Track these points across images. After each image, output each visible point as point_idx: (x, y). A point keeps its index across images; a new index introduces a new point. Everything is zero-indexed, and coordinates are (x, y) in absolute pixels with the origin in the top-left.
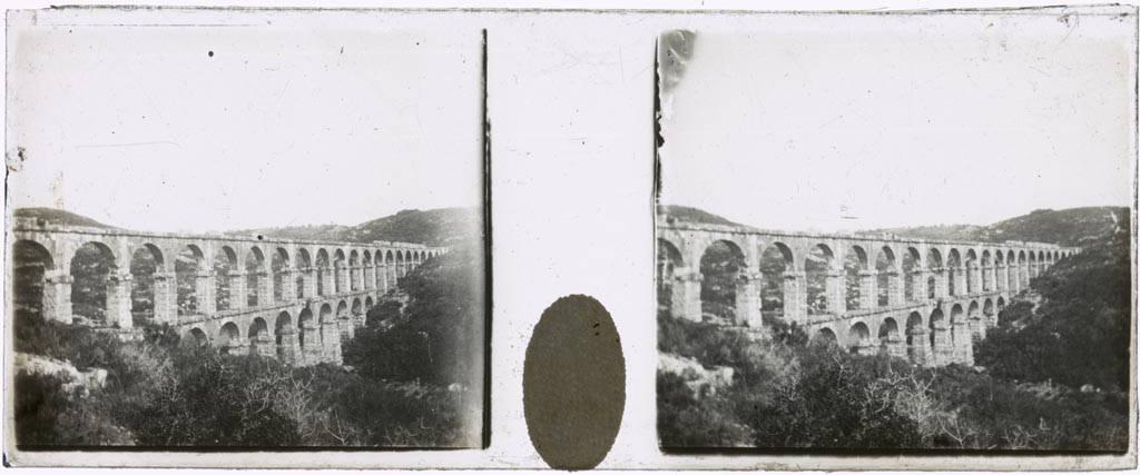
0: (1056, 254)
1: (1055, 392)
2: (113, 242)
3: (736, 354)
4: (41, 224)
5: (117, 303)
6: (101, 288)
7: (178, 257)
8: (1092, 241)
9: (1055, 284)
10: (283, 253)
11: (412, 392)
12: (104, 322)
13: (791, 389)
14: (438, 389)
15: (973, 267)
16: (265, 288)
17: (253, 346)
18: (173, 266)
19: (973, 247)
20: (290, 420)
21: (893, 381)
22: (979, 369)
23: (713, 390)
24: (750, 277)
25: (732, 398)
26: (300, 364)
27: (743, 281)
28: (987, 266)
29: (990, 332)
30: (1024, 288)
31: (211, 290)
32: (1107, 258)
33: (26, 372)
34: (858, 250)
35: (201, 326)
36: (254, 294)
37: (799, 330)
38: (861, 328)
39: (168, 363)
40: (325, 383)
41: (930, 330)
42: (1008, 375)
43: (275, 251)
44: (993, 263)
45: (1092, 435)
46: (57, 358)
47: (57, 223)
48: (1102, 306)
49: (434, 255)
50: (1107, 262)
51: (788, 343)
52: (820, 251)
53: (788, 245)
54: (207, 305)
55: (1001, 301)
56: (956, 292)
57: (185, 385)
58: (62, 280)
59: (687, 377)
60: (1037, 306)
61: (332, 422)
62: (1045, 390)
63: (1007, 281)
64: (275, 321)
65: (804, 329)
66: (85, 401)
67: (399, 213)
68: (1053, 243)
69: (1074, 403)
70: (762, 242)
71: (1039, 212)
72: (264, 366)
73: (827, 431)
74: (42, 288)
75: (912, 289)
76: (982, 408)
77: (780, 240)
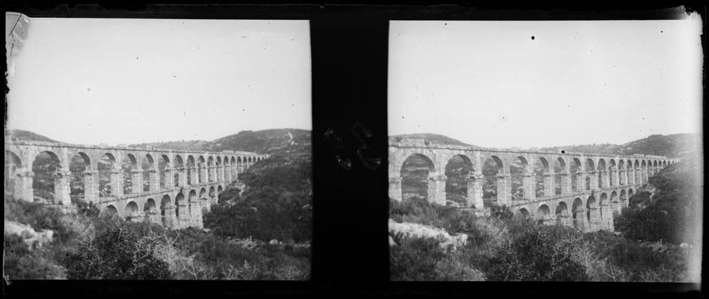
0: (254, 158)
1: (254, 244)
3: (55, 222)
4: (427, 144)
5: (61, 189)
6: (51, 180)
7: (512, 164)
8: (277, 150)
9: (253, 178)
10: (577, 162)
11: (657, 248)
12: (465, 205)
13: (89, 244)
14: (673, 247)
15: (203, 167)
16: (566, 183)
17: (558, 220)
18: (509, 170)
20: (581, 266)
21: (152, 238)
22: (207, 230)
23: (40, 244)
24: (63, 174)
25: (52, 249)
26: (588, 231)
27: (59, 176)
28: (211, 166)
29: (213, 207)
30: (234, 180)
31: (121, 182)
32: (285, 161)
33: (417, 235)
34: (131, 156)
35: (526, 207)
36: (147, 184)
37: (94, 207)
38: (133, 205)
39: (505, 230)
40: (603, 242)
41: (176, 207)
42: (225, 234)
43: (573, 161)
44: (215, 164)
45: (277, 271)
46: (436, 227)
47: (24, 139)
48: (283, 191)
49: (671, 162)
50: (286, 163)
51: (87, 215)
52: (107, 158)
53: (87, 154)
54: (530, 194)
55: (631, 191)
56: (603, 186)
57: (516, 244)
58: (440, 178)
59: (24, 236)
60: (242, 191)
61: (608, 267)
62: (247, 243)
63: (223, 176)
64: (160, 201)
65: (97, 206)
66: (454, 254)
67: (650, 137)
68: (253, 151)
69: (266, 251)
70: (70, 152)
71: (243, 132)
72: (565, 232)
73: (112, 270)
74: (427, 183)
75: (164, 180)
76: (208, 254)
77: (82, 151)
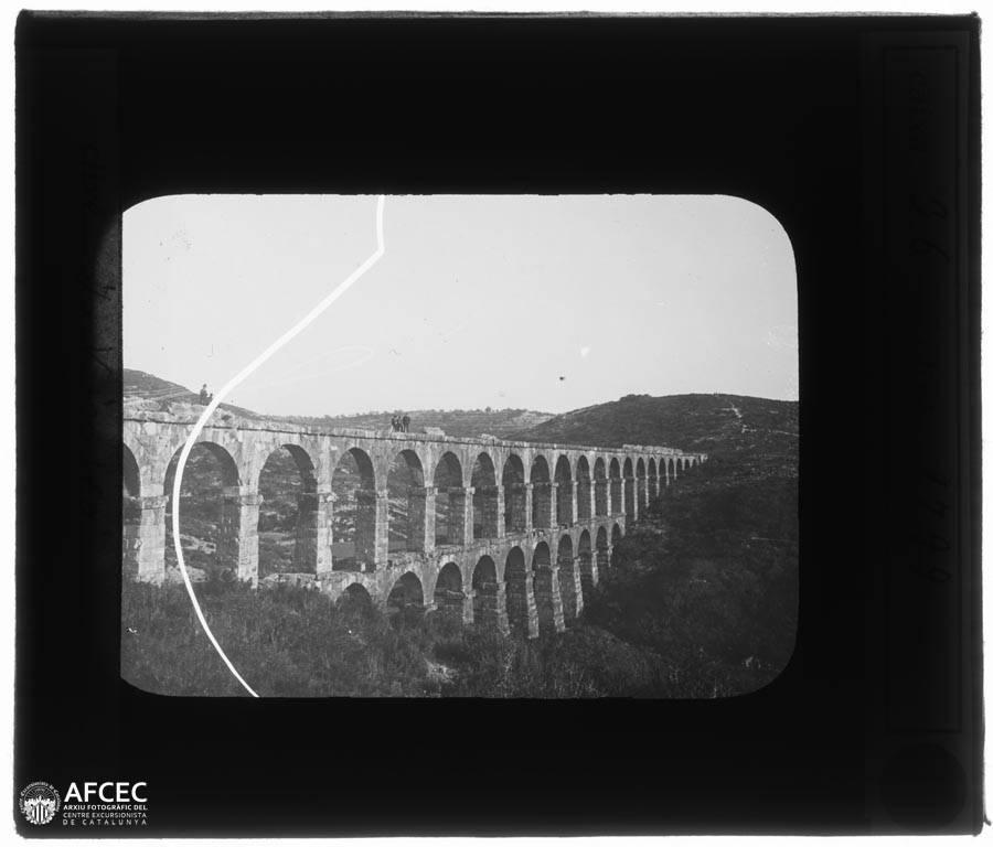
2: (313, 446)
19: (583, 453)
71: (630, 399)
